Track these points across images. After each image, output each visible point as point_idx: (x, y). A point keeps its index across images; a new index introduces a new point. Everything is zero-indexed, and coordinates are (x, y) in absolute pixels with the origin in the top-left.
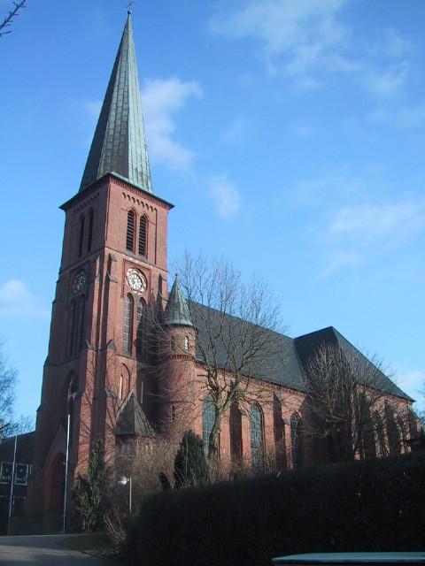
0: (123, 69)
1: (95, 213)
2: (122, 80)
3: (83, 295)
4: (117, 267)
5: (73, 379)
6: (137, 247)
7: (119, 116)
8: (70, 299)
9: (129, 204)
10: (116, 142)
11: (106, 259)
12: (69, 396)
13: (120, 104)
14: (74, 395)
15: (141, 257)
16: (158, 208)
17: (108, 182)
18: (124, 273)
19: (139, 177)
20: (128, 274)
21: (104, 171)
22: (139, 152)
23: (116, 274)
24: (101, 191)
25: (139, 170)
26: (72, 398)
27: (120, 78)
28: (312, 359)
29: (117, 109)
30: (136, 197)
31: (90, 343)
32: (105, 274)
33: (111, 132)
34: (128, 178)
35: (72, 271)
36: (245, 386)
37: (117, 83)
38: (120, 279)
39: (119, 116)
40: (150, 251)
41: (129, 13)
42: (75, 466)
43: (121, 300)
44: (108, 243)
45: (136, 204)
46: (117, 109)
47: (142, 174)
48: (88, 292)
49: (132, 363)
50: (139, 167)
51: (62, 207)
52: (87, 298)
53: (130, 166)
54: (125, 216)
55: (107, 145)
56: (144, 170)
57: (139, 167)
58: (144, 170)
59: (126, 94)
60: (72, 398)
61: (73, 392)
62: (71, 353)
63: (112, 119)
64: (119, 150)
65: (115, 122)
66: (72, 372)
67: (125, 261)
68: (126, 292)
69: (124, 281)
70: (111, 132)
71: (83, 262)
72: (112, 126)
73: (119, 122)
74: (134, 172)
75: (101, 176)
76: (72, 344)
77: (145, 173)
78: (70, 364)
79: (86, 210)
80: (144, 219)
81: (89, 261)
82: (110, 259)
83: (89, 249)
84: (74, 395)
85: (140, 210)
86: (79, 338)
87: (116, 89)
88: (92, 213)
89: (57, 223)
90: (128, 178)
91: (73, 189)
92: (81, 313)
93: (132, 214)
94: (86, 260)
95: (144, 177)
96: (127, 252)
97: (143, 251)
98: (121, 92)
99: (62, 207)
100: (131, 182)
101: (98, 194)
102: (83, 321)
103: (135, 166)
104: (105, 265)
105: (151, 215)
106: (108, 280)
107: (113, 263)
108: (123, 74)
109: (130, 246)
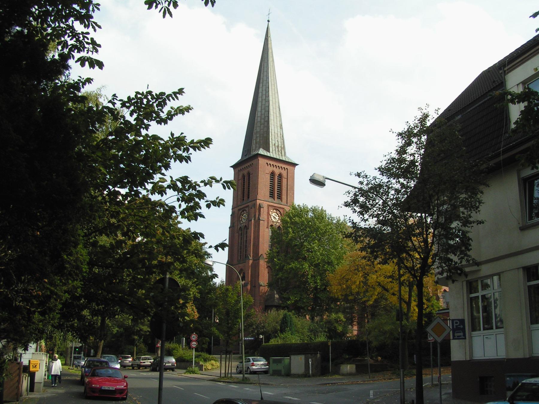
1: (251, 176)
4: (264, 211)
5: (242, 273)
6: (276, 195)
8: (239, 227)
9: (271, 169)
15: (279, 201)
20: (271, 213)
22: (276, 132)
23: (263, 216)
24: (254, 162)
25: (276, 145)
29: (262, 102)
31: (250, 256)
35: (239, 210)
36: (141, 266)
38: (266, 217)
40: (284, 197)
41: (268, 21)
43: (267, 230)
44: (259, 197)
46: (262, 102)
47: (278, 147)
49: (39, 397)
50: (276, 142)
52: (248, 229)
53: (271, 143)
54: (268, 177)
55: (258, 114)
56: (280, 143)
62: (241, 258)
65: (261, 112)
67: (269, 206)
68: (270, 224)
71: (245, 206)
73: (263, 111)
74: (273, 146)
76: (241, 253)
77: (280, 146)
78: (240, 265)
79: (245, 172)
80: (280, 176)
81: (248, 206)
82: (260, 207)
83: (248, 197)
85: (277, 171)
86: (245, 251)
88: (249, 174)
91: (237, 157)
93: (273, 174)
94: (247, 205)
95: (280, 148)
97: (280, 197)
98: (264, 87)
101: (252, 164)
103: (274, 142)
105: (284, 173)
106: (259, 219)
107: (262, 209)
109: (272, 195)
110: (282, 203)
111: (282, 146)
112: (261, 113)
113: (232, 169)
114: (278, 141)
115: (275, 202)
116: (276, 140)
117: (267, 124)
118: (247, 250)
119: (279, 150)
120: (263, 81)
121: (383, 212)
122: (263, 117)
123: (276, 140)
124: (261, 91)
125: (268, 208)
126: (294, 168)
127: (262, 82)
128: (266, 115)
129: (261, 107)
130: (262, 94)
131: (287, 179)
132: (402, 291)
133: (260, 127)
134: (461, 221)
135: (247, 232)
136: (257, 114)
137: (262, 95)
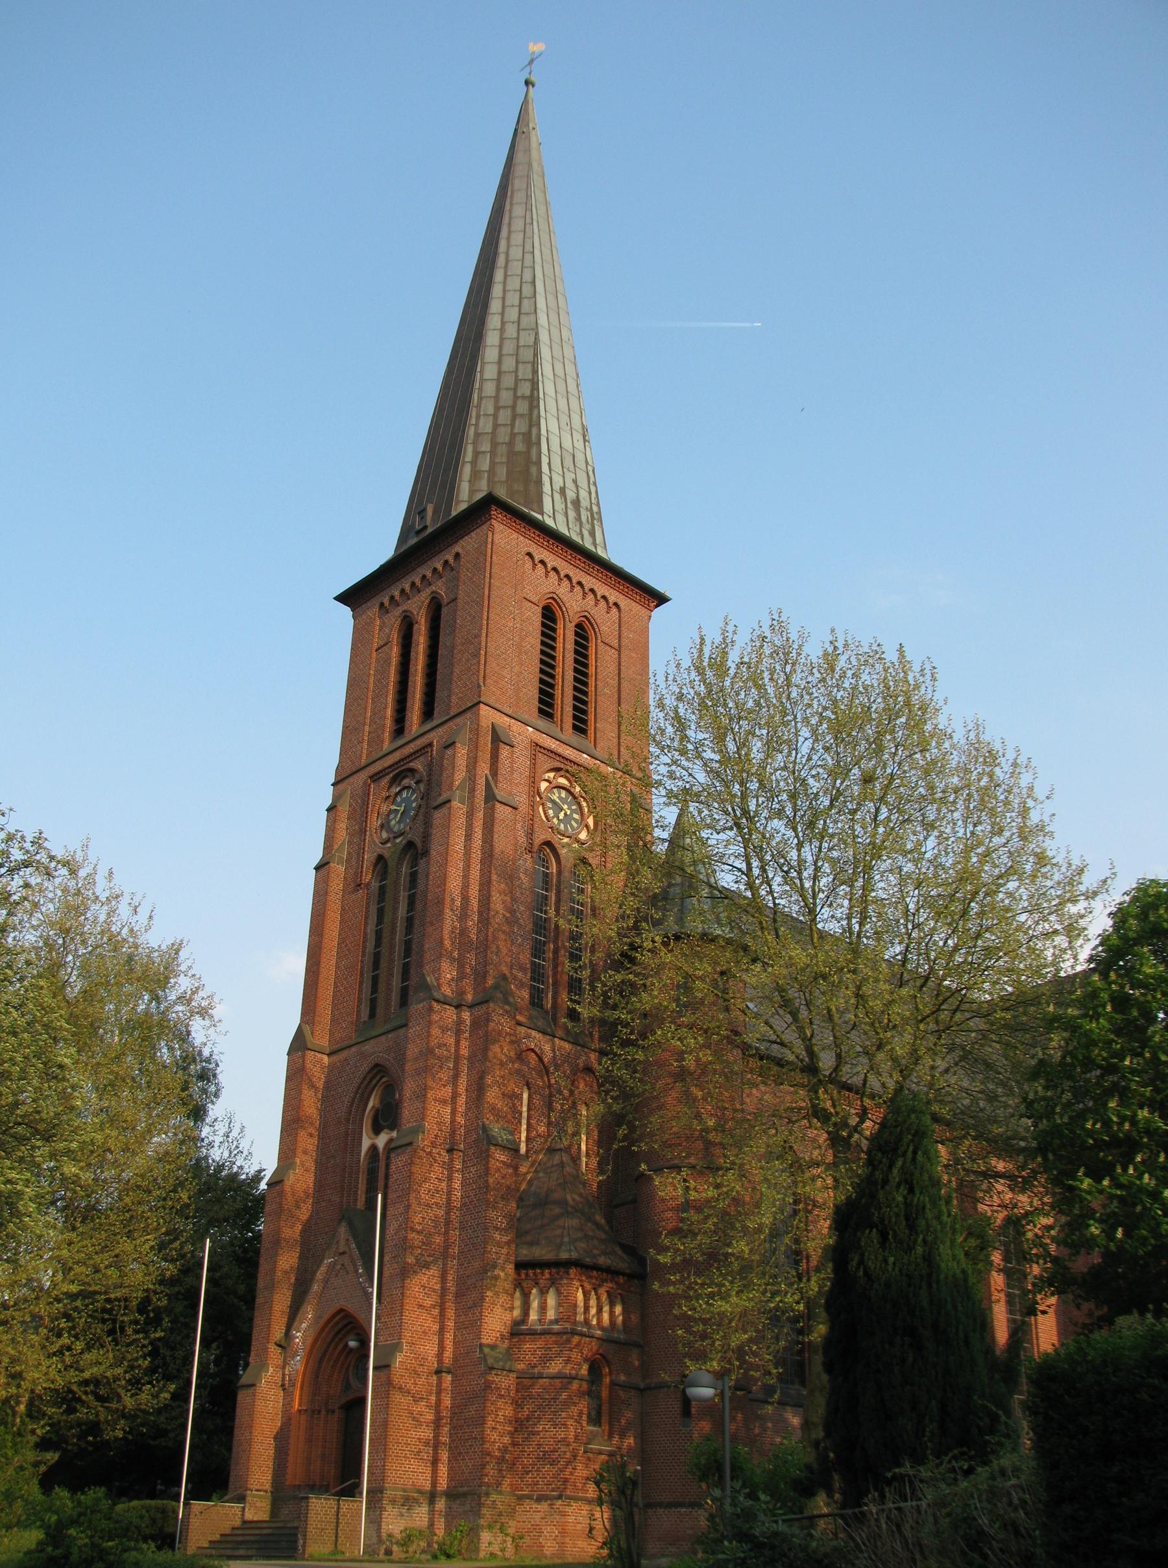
0: (518, 225)
1: (444, 611)
2: (516, 253)
3: (410, 845)
4: (515, 762)
6: (569, 710)
7: (509, 347)
9: (541, 586)
10: (504, 416)
11: (486, 741)
12: (366, 1143)
13: (512, 314)
14: (382, 1140)
15: (575, 739)
16: (624, 602)
17: (489, 511)
18: (533, 783)
19: (572, 514)
20: (544, 785)
21: (472, 492)
23: (511, 785)
24: (466, 545)
25: (571, 495)
26: (374, 1147)
27: (510, 247)
28: (507, 1012)
29: (502, 330)
30: (565, 568)
32: (481, 782)
33: (489, 389)
34: (542, 513)
37: (501, 261)
39: (509, 347)
41: (527, 83)
42: (396, 1347)
45: (563, 590)
46: (502, 330)
47: (577, 503)
48: (426, 837)
50: (570, 485)
51: (346, 598)
52: (426, 853)
53: (546, 479)
54: (537, 620)
55: (480, 421)
57: (570, 485)
58: (583, 494)
59: (527, 290)
60: (374, 1147)
61: (377, 1130)
63: (490, 353)
64: (513, 435)
65: (500, 363)
66: (378, 1070)
69: (533, 807)
70: (489, 389)
71: (407, 750)
72: (490, 372)
73: (509, 364)
74: (557, 497)
75: (463, 506)
77: (585, 503)
78: (368, 1047)
80: (582, 633)
84: (382, 1140)
85: (574, 604)
87: (499, 276)
89: (309, 879)
90: (542, 513)
92: (403, 895)
95: (584, 515)
96: (542, 723)
99: (346, 598)
100: (549, 522)
101: (457, 555)
102: (410, 921)
103: (558, 482)
104: (485, 756)
105: (605, 622)
106: (490, 797)
107: (504, 752)
108: (517, 239)
109: (546, 706)
110: (597, 754)
111: (595, 509)
112: (500, 368)
113: (346, 611)
114: (575, 481)
115: (563, 737)
116: (569, 477)
117: (532, 391)
118: (417, 922)
119: (584, 519)
120: (507, 261)
121: (971, 806)
122: (508, 381)
123: (569, 477)
124: (501, 295)
125: (534, 758)
126: (643, 612)
127: (473, 421)
128: (516, 431)
129: (501, 347)
130: (504, 287)
131: (619, 651)
132: (255, 1519)
133: (495, 416)
134: (1042, 961)
135: (413, 878)
136: (480, 389)
137: (504, 307)
